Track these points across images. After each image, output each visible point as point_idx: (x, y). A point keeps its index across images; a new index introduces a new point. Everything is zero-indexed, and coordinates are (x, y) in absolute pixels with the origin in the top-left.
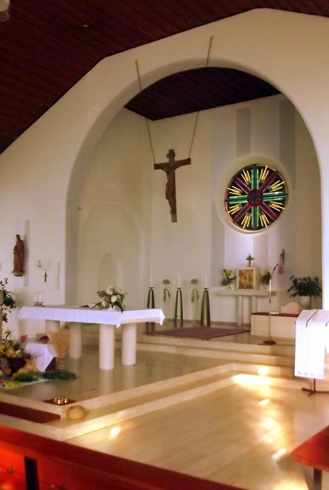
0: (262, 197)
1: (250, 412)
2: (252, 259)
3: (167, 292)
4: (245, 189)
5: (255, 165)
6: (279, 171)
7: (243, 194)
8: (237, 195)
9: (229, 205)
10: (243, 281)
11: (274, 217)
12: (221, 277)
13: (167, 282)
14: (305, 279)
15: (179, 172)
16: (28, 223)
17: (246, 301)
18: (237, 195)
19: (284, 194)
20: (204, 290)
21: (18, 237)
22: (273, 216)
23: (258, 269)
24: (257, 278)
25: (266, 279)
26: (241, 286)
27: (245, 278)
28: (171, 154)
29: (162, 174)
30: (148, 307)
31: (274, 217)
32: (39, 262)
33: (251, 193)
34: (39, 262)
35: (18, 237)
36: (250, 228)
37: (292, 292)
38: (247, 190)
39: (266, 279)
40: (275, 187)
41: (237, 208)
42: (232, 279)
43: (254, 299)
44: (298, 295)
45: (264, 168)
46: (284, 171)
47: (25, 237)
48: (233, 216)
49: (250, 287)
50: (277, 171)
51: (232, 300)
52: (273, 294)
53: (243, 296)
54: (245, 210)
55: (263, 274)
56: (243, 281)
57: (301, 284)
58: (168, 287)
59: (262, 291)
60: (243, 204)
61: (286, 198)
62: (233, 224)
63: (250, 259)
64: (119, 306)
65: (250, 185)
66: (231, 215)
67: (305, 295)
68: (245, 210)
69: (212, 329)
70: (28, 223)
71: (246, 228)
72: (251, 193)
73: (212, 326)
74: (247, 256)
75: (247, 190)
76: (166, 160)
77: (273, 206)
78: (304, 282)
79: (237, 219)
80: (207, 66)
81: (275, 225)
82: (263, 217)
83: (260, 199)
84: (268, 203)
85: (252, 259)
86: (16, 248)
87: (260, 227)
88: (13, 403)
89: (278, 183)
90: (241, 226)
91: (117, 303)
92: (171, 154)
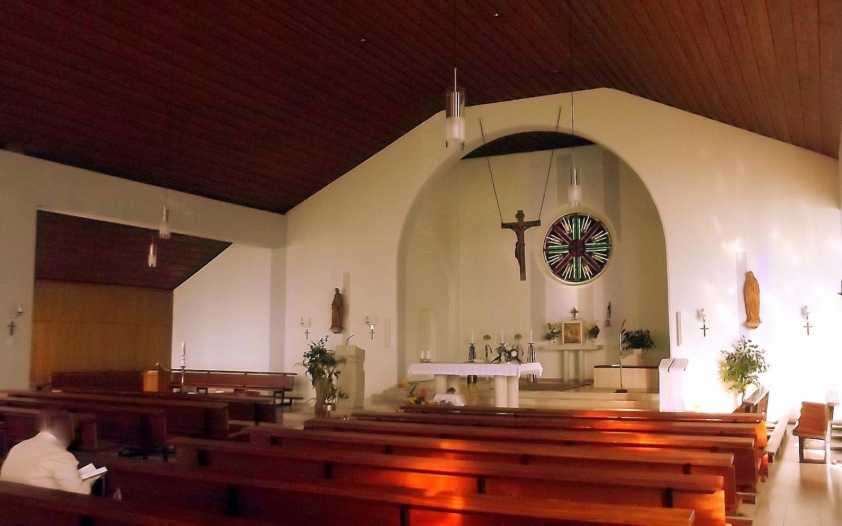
0: (585, 247)
1: (731, 383)
2: (577, 312)
3: (488, 347)
4: (565, 238)
5: (576, 214)
6: (602, 221)
7: (564, 243)
8: (558, 245)
9: (548, 255)
10: (569, 335)
11: (598, 269)
12: (542, 332)
13: (487, 337)
14: (637, 332)
15: (527, 233)
16: (347, 277)
17: (572, 355)
18: (558, 245)
19: (608, 245)
20: (471, 345)
21: (337, 290)
22: (597, 268)
23: (584, 322)
24: (584, 332)
25: (594, 332)
26: (568, 341)
27: (571, 333)
28: (520, 215)
29: (512, 234)
30: (530, 362)
31: (598, 269)
32: (367, 318)
33: (571, 243)
34: (367, 318)
35: (337, 290)
36: (572, 280)
37: (625, 345)
38: (569, 240)
39: (594, 332)
40: (598, 237)
41: (557, 258)
42: (556, 333)
43: (581, 353)
44: (631, 348)
45: (586, 217)
46: (607, 221)
47: (344, 290)
48: (553, 267)
49: (577, 341)
50: (600, 222)
51: (556, 356)
52: (600, 348)
53: (583, 350)
54: (567, 261)
55: (590, 328)
56: (569, 335)
57: (633, 337)
58: (488, 342)
59: (589, 344)
60: (564, 255)
61: (611, 250)
62: (553, 274)
63: (574, 312)
64: (518, 360)
65: (571, 235)
66: (593, 276)
67: (639, 348)
68: (588, 259)
69: (231, 387)
70: (347, 277)
71: (568, 279)
72: (571, 243)
73: (538, 382)
74: (572, 308)
75: (569, 240)
76: (515, 220)
77: (596, 257)
78: (637, 335)
79: (558, 270)
80: (485, 143)
81: (599, 279)
82: (587, 268)
83: (583, 249)
84: (591, 254)
85: (577, 312)
86: (334, 304)
87: (583, 279)
88: (349, 306)
89: (602, 234)
90: (563, 278)
91: (516, 358)
92: (520, 215)
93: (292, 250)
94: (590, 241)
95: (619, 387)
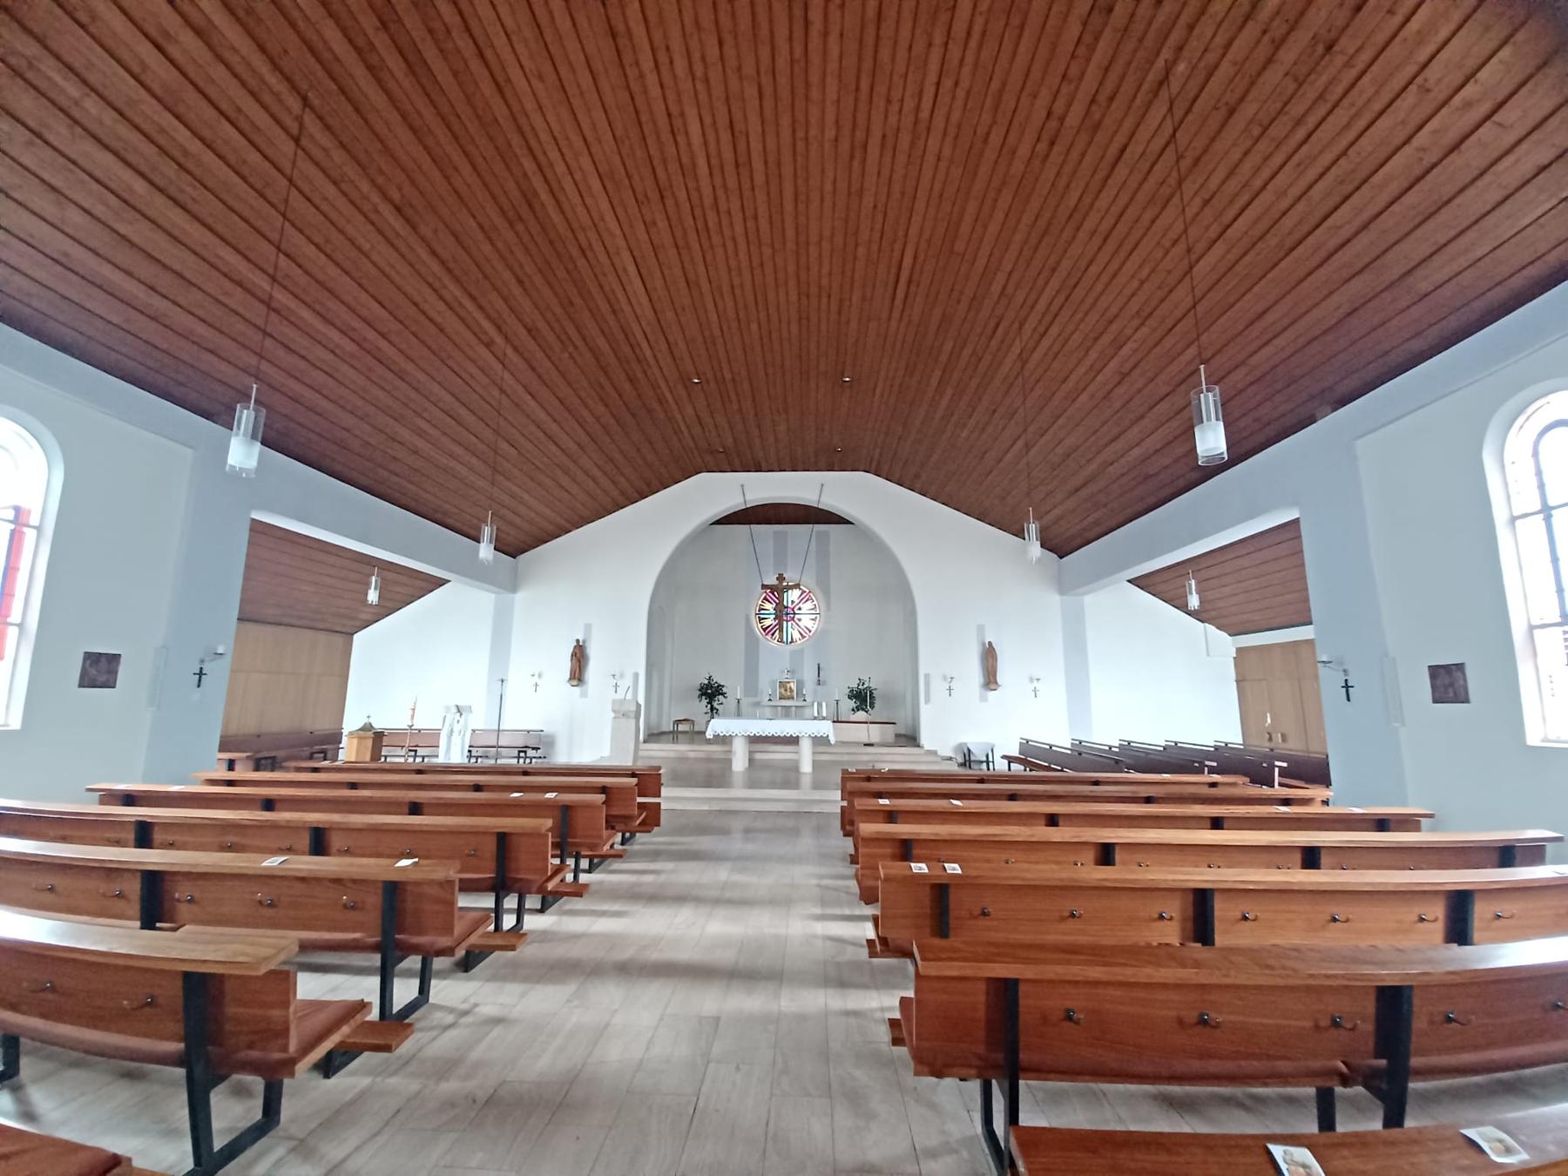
16: (588, 628)
47: (584, 642)
70: (588, 628)
93: (520, 597)
94: (800, 609)
95: (867, 741)
